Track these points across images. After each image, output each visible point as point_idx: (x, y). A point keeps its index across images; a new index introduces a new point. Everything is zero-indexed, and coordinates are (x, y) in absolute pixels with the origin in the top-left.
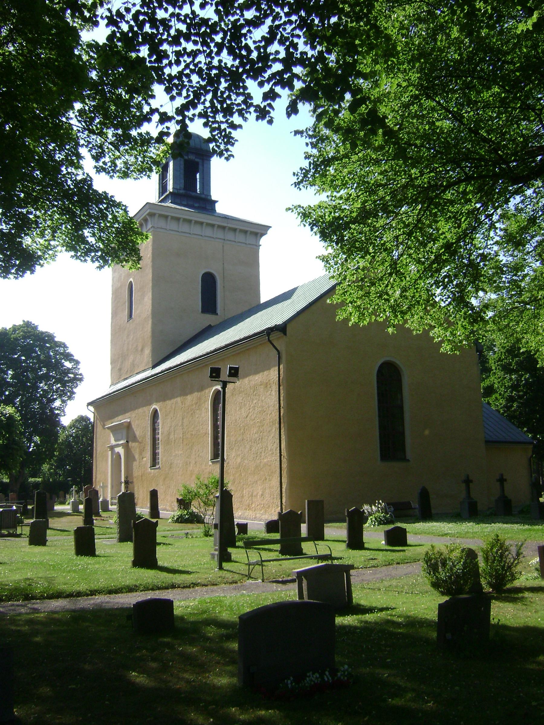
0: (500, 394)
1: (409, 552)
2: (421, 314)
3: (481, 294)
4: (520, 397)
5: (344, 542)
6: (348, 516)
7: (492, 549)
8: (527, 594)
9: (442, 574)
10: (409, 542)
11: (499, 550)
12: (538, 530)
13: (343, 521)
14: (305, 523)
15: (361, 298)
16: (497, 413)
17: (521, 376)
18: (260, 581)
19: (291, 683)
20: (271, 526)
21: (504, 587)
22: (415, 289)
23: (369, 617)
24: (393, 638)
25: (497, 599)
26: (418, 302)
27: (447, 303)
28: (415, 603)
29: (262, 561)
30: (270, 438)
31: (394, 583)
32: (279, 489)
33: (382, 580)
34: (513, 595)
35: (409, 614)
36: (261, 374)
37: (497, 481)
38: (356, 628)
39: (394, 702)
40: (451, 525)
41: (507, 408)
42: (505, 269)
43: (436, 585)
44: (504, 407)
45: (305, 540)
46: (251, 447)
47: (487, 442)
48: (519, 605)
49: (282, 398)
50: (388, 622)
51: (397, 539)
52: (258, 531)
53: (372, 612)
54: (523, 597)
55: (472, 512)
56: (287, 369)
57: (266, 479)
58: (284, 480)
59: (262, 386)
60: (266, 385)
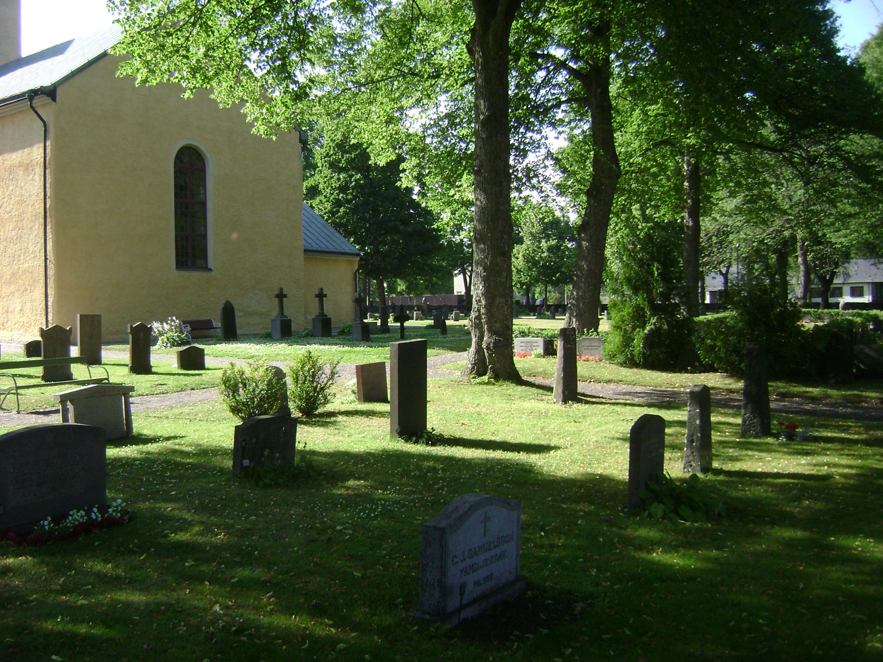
0: (326, 197)
1: (206, 376)
2: (232, 83)
3: (308, 66)
4: (349, 202)
5: (127, 365)
6: (131, 333)
7: (303, 367)
8: (340, 418)
9: (242, 395)
10: (206, 366)
11: (311, 372)
12: (359, 352)
13: (124, 342)
14: (76, 345)
15: (152, 51)
16: (320, 219)
17: (352, 176)
18: (14, 412)
19: (49, 524)
20: (32, 348)
21: (313, 411)
22: (225, 48)
23: (151, 447)
24: (180, 471)
25: (305, 423)
26: (228, 67)
27: (265, 71)
28: (209, 431)
29: (18, 388)
30: (32, 237)
31: (186, 410)
32: (44, 303)
33: (172, 408)
34: (326, 419)
35: (201, 442)
36: (20, 152)
37: (316, 296)
38: (135, 459)
39: (177, 537)
40: (258, 347)
41: (333, 213)
42: (339, 40)
43: (235, 410)
44: (329, 212)
45: (76, 360)
46: (6, 247)
47: (306, 251)
48: (331, 430)
49: (48, 185)
50: (174, 452)
51: (192, 361)
52: (15, 355)
53: (155, 442)
54: (335, 421)
55: (285, 332)
56: (57, 148)
57: (26, 290)
58: (51, 291)
59: (21, 168)
60: (27, 167)
